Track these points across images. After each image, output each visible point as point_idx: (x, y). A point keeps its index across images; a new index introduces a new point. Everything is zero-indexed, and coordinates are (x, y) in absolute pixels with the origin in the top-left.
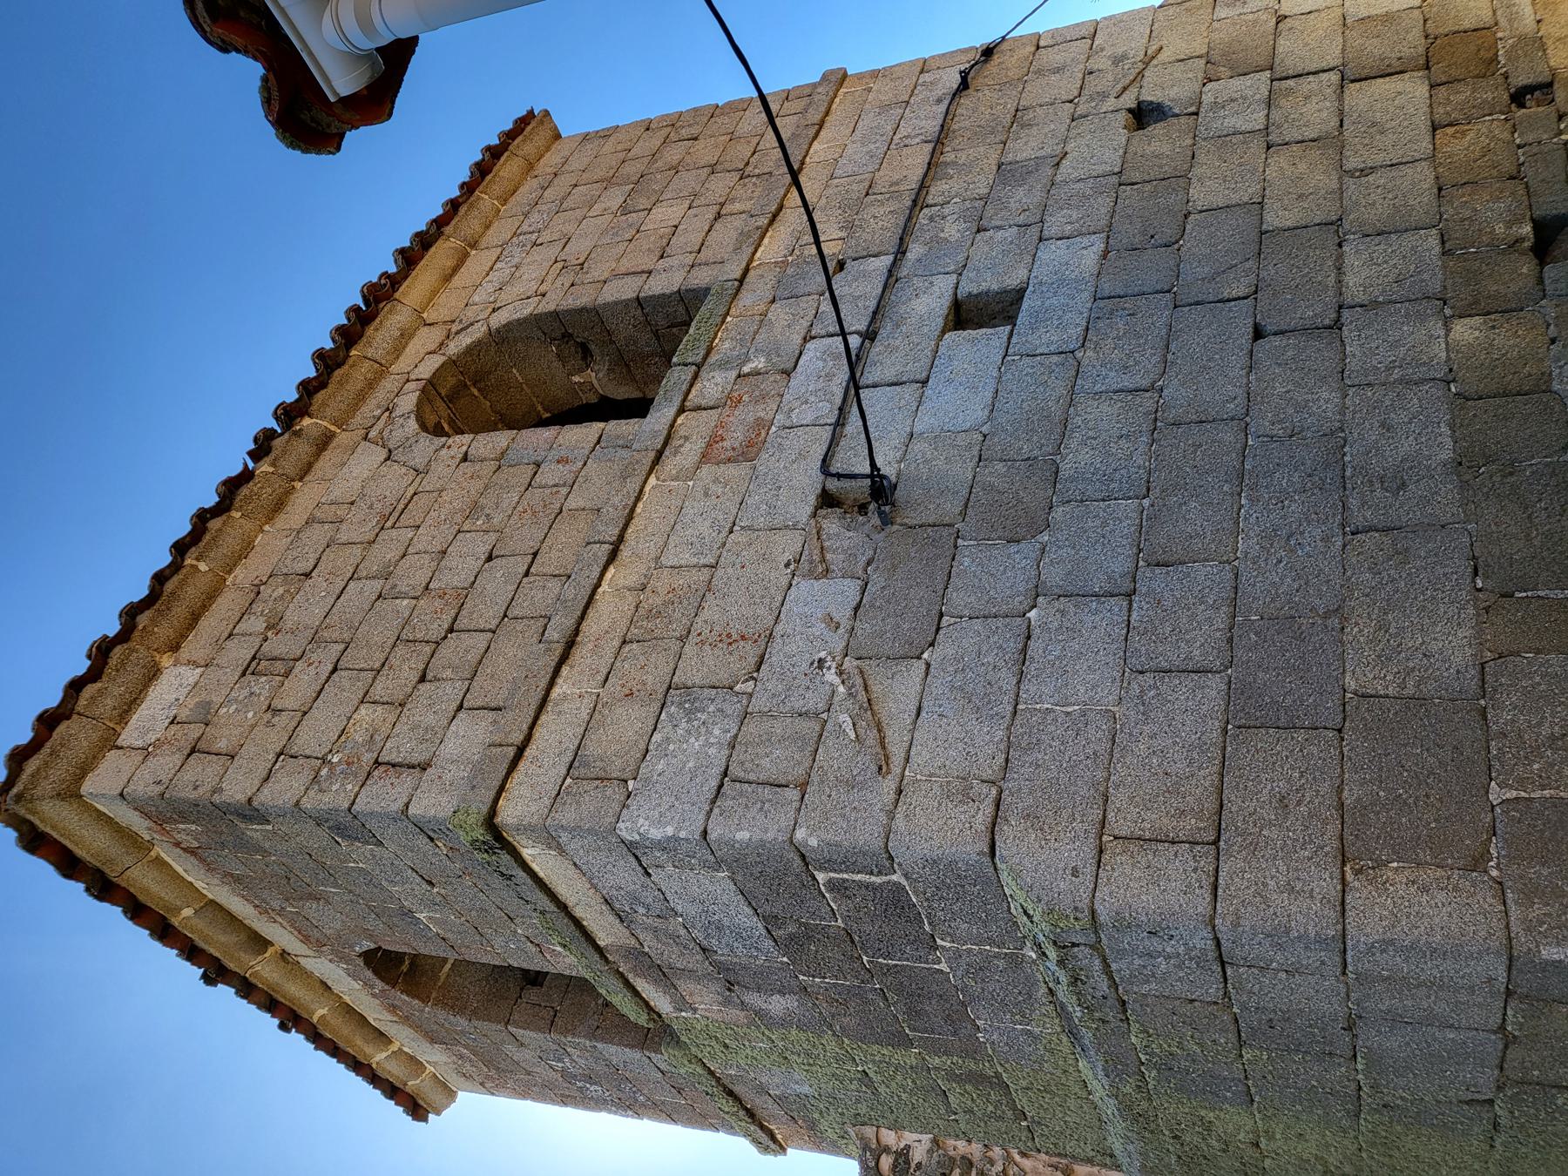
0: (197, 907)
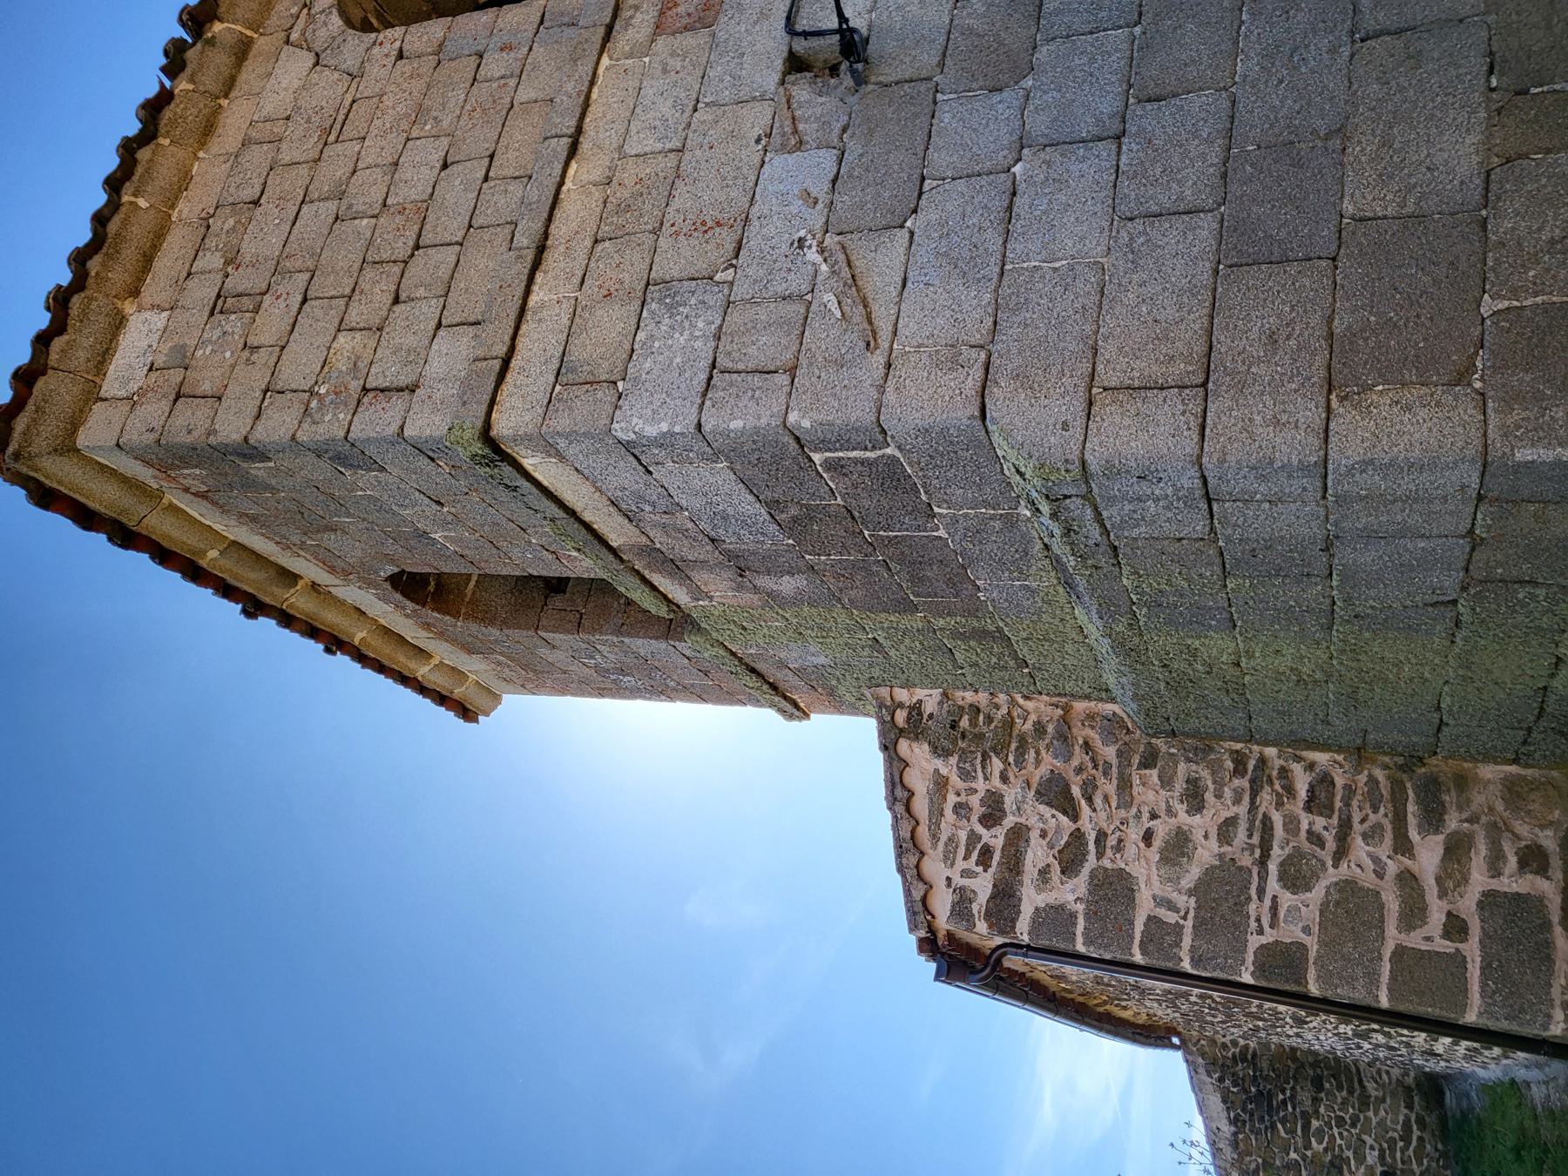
0: (221, 549)
